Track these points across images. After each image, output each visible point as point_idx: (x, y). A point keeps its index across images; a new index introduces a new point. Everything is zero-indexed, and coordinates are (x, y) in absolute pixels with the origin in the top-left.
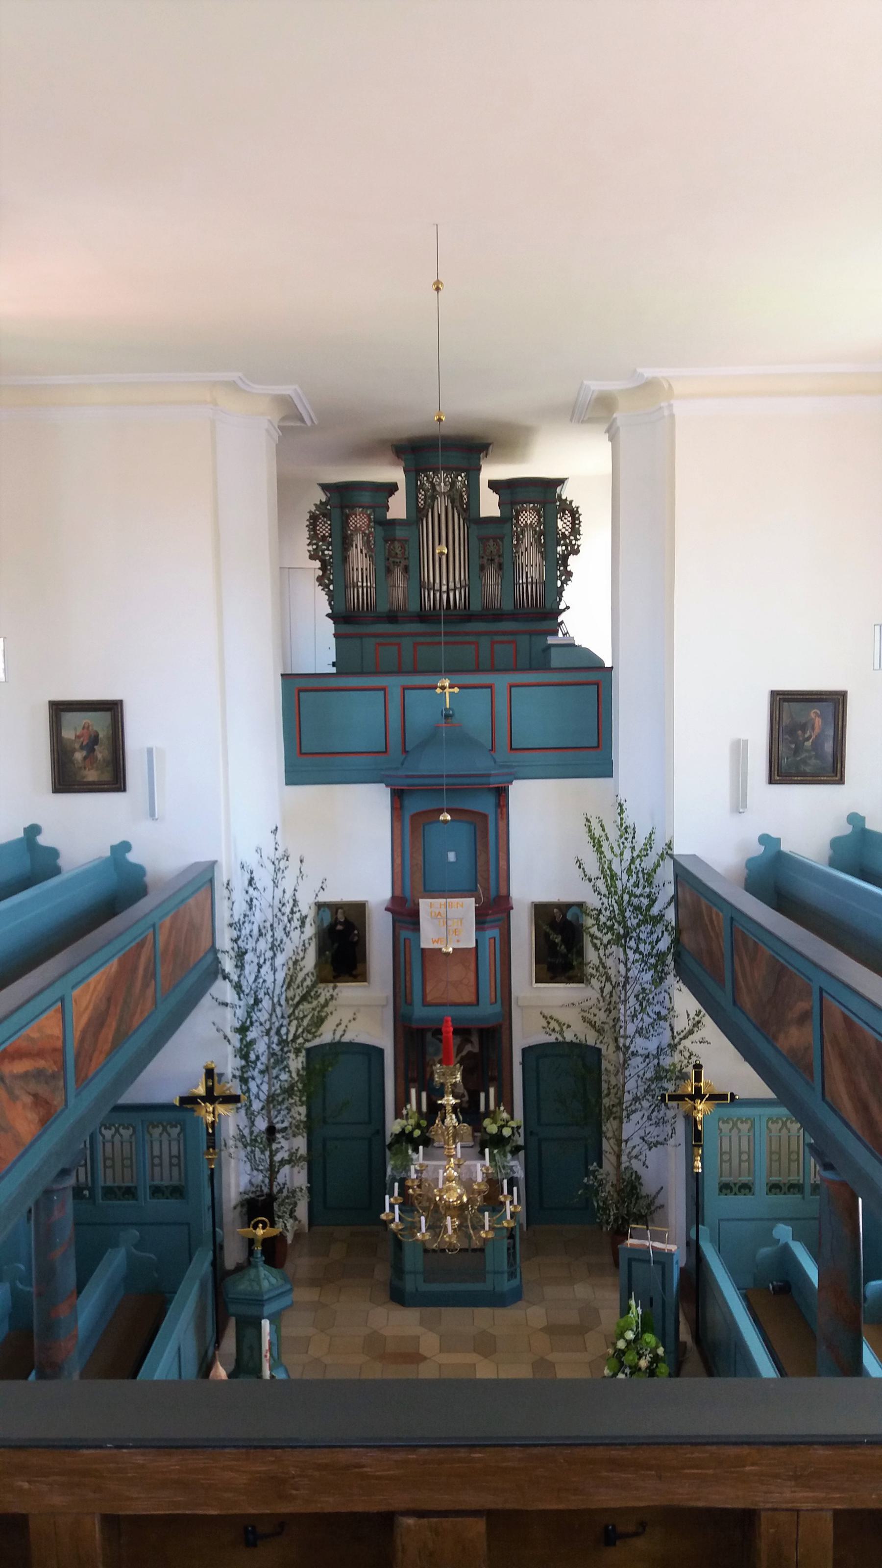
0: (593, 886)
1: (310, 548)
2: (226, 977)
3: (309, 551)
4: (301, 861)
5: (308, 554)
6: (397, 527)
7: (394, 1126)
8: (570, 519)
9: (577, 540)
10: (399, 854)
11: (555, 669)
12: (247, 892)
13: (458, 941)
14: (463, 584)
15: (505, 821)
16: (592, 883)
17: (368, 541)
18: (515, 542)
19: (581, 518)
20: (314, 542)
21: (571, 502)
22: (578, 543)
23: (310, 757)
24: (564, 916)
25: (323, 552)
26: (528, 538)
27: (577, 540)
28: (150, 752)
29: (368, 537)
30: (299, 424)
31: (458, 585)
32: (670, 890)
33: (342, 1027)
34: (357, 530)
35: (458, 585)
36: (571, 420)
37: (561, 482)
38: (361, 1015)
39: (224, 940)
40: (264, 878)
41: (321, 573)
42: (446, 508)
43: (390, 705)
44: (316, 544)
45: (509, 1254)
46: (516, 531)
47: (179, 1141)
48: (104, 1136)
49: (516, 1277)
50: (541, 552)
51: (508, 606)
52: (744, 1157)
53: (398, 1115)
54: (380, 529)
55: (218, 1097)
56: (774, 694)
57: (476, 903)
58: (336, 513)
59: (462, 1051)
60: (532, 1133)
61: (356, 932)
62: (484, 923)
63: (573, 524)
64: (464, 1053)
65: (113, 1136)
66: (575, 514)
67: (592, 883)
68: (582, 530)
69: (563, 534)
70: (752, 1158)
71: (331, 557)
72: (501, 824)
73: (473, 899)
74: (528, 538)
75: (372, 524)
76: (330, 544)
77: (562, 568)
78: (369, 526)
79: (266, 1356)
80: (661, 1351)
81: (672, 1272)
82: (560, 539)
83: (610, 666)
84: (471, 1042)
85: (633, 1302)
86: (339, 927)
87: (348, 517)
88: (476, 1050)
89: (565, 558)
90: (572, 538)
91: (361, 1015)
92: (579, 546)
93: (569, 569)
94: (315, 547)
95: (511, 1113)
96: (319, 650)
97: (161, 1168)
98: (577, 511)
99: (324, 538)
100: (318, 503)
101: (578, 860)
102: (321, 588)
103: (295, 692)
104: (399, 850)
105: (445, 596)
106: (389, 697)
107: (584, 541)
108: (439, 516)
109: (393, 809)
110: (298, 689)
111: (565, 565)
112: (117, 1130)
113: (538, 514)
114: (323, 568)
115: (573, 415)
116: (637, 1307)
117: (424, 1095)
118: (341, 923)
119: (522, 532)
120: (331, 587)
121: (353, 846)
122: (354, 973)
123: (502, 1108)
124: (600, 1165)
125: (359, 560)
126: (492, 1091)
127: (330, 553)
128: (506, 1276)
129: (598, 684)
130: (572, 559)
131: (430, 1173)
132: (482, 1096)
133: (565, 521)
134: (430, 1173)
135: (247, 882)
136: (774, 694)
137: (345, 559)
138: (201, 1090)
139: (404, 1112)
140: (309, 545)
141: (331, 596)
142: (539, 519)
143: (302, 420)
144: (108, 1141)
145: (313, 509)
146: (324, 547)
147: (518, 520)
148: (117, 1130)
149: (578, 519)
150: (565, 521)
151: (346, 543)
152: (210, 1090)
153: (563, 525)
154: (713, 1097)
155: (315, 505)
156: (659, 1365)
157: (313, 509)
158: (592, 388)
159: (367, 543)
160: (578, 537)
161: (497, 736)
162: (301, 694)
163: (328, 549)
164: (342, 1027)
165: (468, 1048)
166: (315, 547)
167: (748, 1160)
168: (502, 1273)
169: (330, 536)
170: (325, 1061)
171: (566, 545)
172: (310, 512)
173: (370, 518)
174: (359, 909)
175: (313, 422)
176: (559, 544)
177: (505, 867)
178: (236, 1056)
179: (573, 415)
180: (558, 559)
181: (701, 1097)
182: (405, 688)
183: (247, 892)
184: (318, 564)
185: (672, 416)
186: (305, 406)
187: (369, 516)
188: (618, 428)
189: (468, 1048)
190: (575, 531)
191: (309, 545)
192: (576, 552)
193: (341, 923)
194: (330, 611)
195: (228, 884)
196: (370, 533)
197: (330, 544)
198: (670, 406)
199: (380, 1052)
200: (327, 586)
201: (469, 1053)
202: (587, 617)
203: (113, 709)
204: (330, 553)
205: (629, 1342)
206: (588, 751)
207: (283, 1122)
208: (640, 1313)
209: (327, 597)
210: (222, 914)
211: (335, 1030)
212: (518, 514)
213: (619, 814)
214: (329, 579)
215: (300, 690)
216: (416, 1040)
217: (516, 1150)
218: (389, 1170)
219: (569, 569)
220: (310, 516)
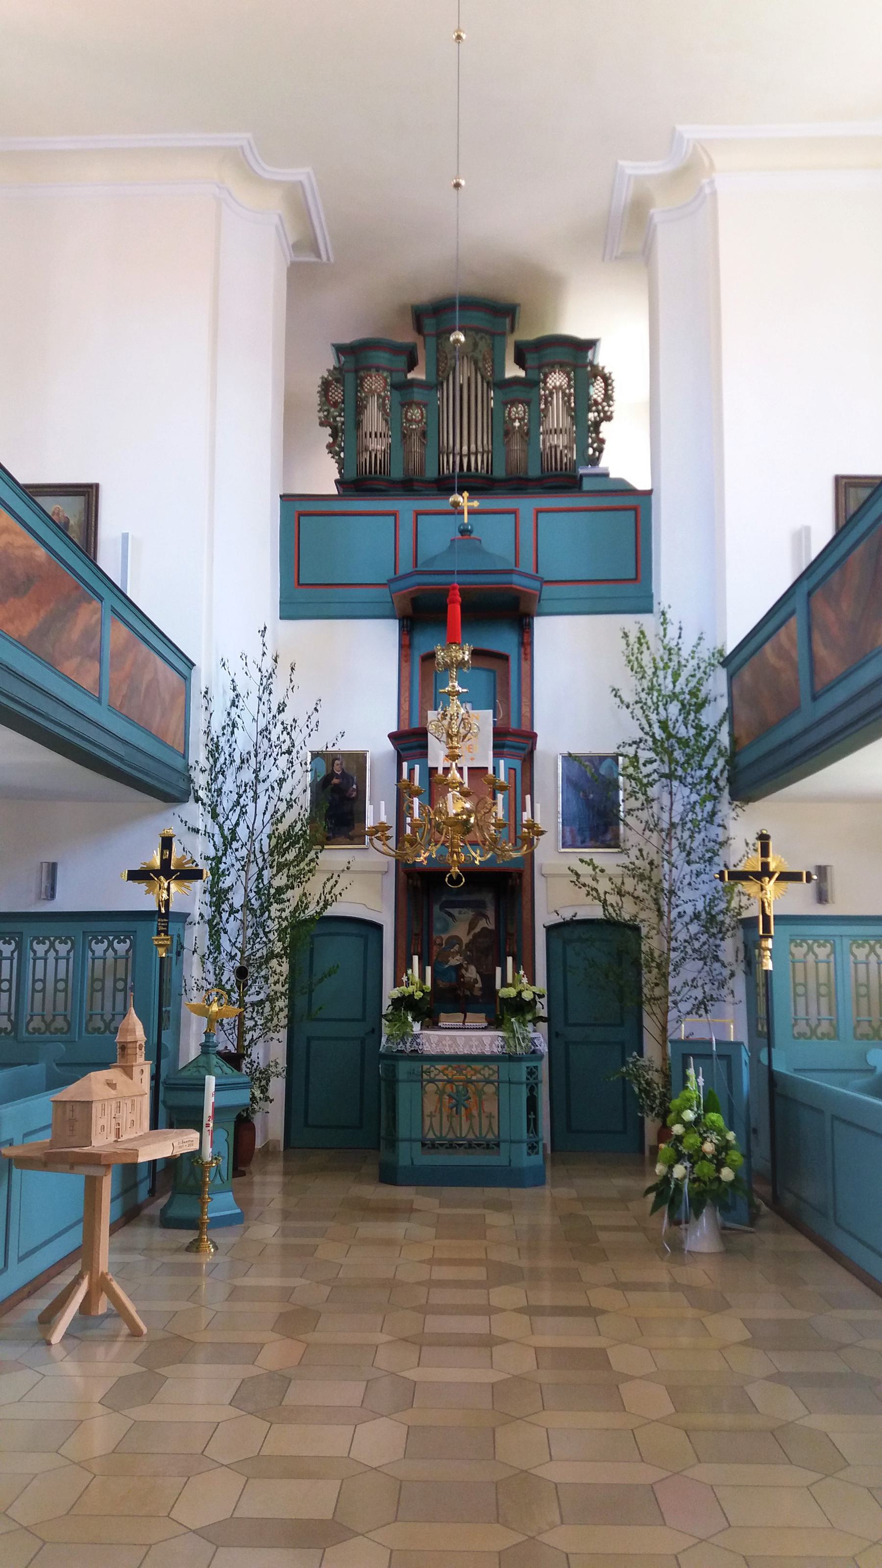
0: (632, 713)
1: (321, 414)
2: (198, 799)
3: (320, 418)
4: (292, 669)
5: (318, 421)
6: (416, 390)
7: (390, 992)
8: (603, 384)
9: (609, 406)
10: (407, 699)
11: (588, 492)
12: (229, 714)
13: (472, 759)
14: (486, 449)
15: (529, 662)
16: (630, 710)
17: (384, 405)
18: (543, 406)
19: (614, 384)
20: (326, 408)
21: (603, 368)
22: (611, 409)
23: (307, 592)
24: (597, 770)
25: (335, 418)
26: (557, 401)
27: (609, 406)
28: (125, 537)
29: (384, 400)
30: (313, 259)
31: (480, 449)
32: (723, 704)
33: (332, 882)
34: (372, 392)
35: (480, 449)
36: (603, 260)
37: (591, 344)
38: (359, 885)
39: (199, 755)
40: (250, 685)
41: (331, 440)
42: (469, 379)
43: (401, 532)
44: (328, 411)
45: (528, 1120)
46: (545, 395)
47: (127, 959)
48: (35, 952)
49: (537, 1153)
50: (572, 417)
51: (534, 472)
52: (823, 990)
53: (397, 983)
54: (396, 393)
55: (175, 871)
56: (838, 479)
57: (494, 717)
58: (350, 378)
59: (473, 929)
60: (557, 1035)
61: (354, 786)
62: (503, 746)
63: (606, 390)
64: (477, 930)
65: (47, 952)
66: (607, 380)
67: (630, 710)
68: (616, 395)
69: (596, 401)
70: (833, 990)
71: (343, 423)
72: (525, 665)
73: (491, 711)
74: (557, 401)
75: (388, 388)
76: (343, 410)
77: (594, 435)
78: (384, 389)
79: (208, 1125)
80: (731, 1136)
81: (741, 1077)
82: (591, 406)
83: (648, 487)
84: (487, 917)
85: (691, 1072)
86: (335, 781)
87: (362, 379)
88: (492, 926)
89: (597, 425)
90: (605, 404)
91: (359, 885)
92: (612, 412)
93: (601, 436)
94: (326, 413)
95: (532, 982)
96: (322, 477)
97: (103, 994)
98: (610, 378)
99: (335, 404)
100: (332, 368)
101: (614, 690)
102: (330, 455)
103: (297, 516)
104: (407, 694)
105: (465, 460)
106: (400, 523)
107: (618, 407)
108: (461, 386)
109: (401, 646)
110: (297, 510)
111: (597, 432)
112: (52, 945)
113: (568, 376)
114: (334, 435)
115: (604, 256)
116: (697, 1078)
117: (429, 969)
118: (337, 777)
119: (551, 394)
120: (342, 455)
121: (353, 686)
122: (351, 833)
123: (522, 972)
124: (641, 1054)
125: (374, 418)
126: (510, 960)
127: (343, 419)
128: (525, 1147)
129: (635, 509)
130: (604, 426)
131: (434, 1045)
132: (498, 970)
133: (597, 387)
134: (434, 1045)
135: (229, 704)
136: (838, 479)
137: (358, 424)
138: (157, 863)
139: (405, 979)
140: (319, 411)
141: (341, 464)
142: (569, 382)
143: (319, 256)
144: (40, 958)
145: (326, 375)
146: (336, 413)
147: (545, 383)
148: (52, 945)
149: (611, 385)
150: (597, 387)
151: (360, 409)
152: (165, 862)
153: (596, 391)
154: (785, 877)
155: (329, 371)
156: (729, 1152)
157: (326, 375)
158: (629, 171)
159: (382, 407)
160: (611, 403)
161: (521, 556)
162: (302, 518)
163: (340, 416)
164: (332, 882)
165: (482, 924)
166: (326, 413)
167: (829, 994)
168: (520, 1142)
169: (343, 402)
170: (315, 936)
171: (598, 411)
172: (323, 378)
173: (386, 382)
174: (359, 759)
175: (328, 259)
176: (590, 410)
177: (528, 714)
178: (205, 892)
179: (604, 256)
180: (589, 427)
181: (771, 875)
182: (418, 514)
183: (229, 714)
184: (328, 430)
185: (714, 193)
186: (320, 218)
187: (385, 379)
188: (655, 226)
189: (482, 924)
190: (608, 397)
191: (319, 411)
192: (609, 418)
193: (337, 777)
194: (338, 477)
195: (206, 693)
196: (386, 396)
197: (343, 410)
198: (712, 182)
199: (378, 928)
200: (338, 454)
201: (484, 929)
202: (624, 454)
203: (88, 494)
204: (343, 419)
205: (687, 1125)
206: (626, 585)
207: (258, 993)
208: (701, 1084)
209: (337, 465)
210: (198, 721)
211: (325, 884)
212: (546, 376)
213: (662, 624)
214: (340, 446)
215: (301, 514)
216: (420, 888)
217: (537, 1019)
218: (384, 1040)
219: (601, 436)
220: (323, 383)
